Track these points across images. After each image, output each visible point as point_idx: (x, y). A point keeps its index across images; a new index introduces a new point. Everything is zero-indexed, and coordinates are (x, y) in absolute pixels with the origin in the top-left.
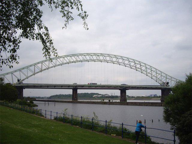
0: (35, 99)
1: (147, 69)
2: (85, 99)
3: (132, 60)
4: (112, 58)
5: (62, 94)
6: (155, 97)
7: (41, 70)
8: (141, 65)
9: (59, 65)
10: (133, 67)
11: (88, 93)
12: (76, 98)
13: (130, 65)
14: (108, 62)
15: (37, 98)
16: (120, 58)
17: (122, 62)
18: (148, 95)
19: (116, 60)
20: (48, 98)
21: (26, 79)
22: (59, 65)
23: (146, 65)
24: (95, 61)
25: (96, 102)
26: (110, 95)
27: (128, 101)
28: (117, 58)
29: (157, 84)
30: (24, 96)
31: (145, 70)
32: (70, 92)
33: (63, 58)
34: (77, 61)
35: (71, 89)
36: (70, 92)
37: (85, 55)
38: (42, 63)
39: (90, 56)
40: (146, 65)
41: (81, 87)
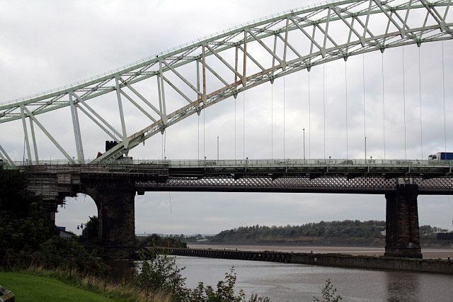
0: (185, 245)
2: (349, 244)
4: (363, 18)
5: (261, 225)
9: (183, 114)
11: (357, 223)
12: (411, 241)
14: (419, 43)
15: (193, 239)
16: (327, 20)
17: (393, 29)
19: (391, 19)
20: (212, 240)
22: (183, 114)
24: (345, 57)
27: (428, 253)
28: (354, 16)
30: (420, 225)
36: (372, 208)
37: (275, 28)
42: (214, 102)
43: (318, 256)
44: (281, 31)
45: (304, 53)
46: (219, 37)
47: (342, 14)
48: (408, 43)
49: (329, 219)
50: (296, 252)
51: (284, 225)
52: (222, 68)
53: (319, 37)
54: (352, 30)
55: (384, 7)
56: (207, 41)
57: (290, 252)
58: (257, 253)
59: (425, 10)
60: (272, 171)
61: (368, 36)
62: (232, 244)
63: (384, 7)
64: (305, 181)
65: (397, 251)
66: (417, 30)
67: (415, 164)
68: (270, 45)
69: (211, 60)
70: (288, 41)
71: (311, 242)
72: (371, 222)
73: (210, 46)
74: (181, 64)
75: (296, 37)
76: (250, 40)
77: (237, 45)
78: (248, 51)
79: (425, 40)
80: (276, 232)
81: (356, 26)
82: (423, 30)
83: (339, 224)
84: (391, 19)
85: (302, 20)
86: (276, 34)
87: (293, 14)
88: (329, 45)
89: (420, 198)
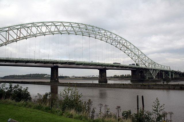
3: (69, 24)
16: (41, 26)
17: (47, 31)
19: (47, 28)
28: (38, 26)
34: (20, 38)
36: (47, 71)
37: (17, 27)
42: (11, 43)
43: (37, 82)
44: (19, 28)
45: (35, 33)
46: (13, 26)
47: (35, 26)
48: (51, 34)
49: (32, 73)
50: (30, 81)
51: (21, 75)
52: (13, 35)
53: (29, 31)
54: (37, 30)
55: (45, 25)
56: (10, 27)
57: (29, 81)
58: (20, 82)
59: (55, 27)
60: (15, 61)
61: (41, 32)
62: (12, 79)
63: (45, 25)
64: (24, 64)
65: (53, 81)
66: (53, 31)
67: (87, 62)
68: (37, 28)
69: (11, 32)
70: (21, 31)
71: (28, 78)
72: (42, 74)
73: (11, 28)
74: (1, 32)
75: (23, 30)
76: (10, 30)
77: (6, 31)
78: (9, 33)
79: (63, 33)
80: (19, 76)
81: (39, 29)
82: (62, 31)
83: (34, 74)
84: (47, 28)
85: (25, 26)
86: (18, 29)
87: (33, 23)
88: (32, 34)
89: (59, 68)
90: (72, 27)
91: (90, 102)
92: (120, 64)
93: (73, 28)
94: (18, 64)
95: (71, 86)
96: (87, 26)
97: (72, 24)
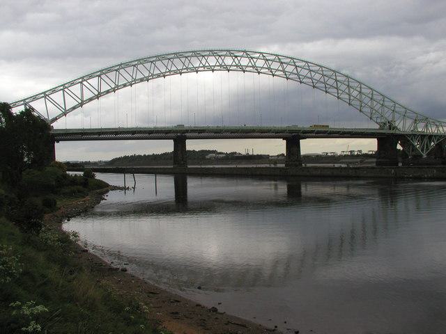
1: (298, 69)
3: (304, 63)
6: (372, 162)
7: (80, 102)
8: (296, 67)
10: (277, 73)
13: (284, 71)
18: (108, 157)
21: (60, 116)
23: (295, 60)
25: (253, 168)
26: (243, 153)
29: (374, 126)
31: (281, 68)
32: (167, 147)
33: (134, 66)
34: (153, 76)
35: (171, 139)
38: (81, 83)
39: (183, 59)
40: (295, 60)
41: (147, 135)
51: (151, 154)
90: (348, 86)
91: (104, 199)
92: (328, 126)
93: (349, 90)
94: (135, 135)
95: (133, 171)
96: (386, 99)
97: (363, 86)
